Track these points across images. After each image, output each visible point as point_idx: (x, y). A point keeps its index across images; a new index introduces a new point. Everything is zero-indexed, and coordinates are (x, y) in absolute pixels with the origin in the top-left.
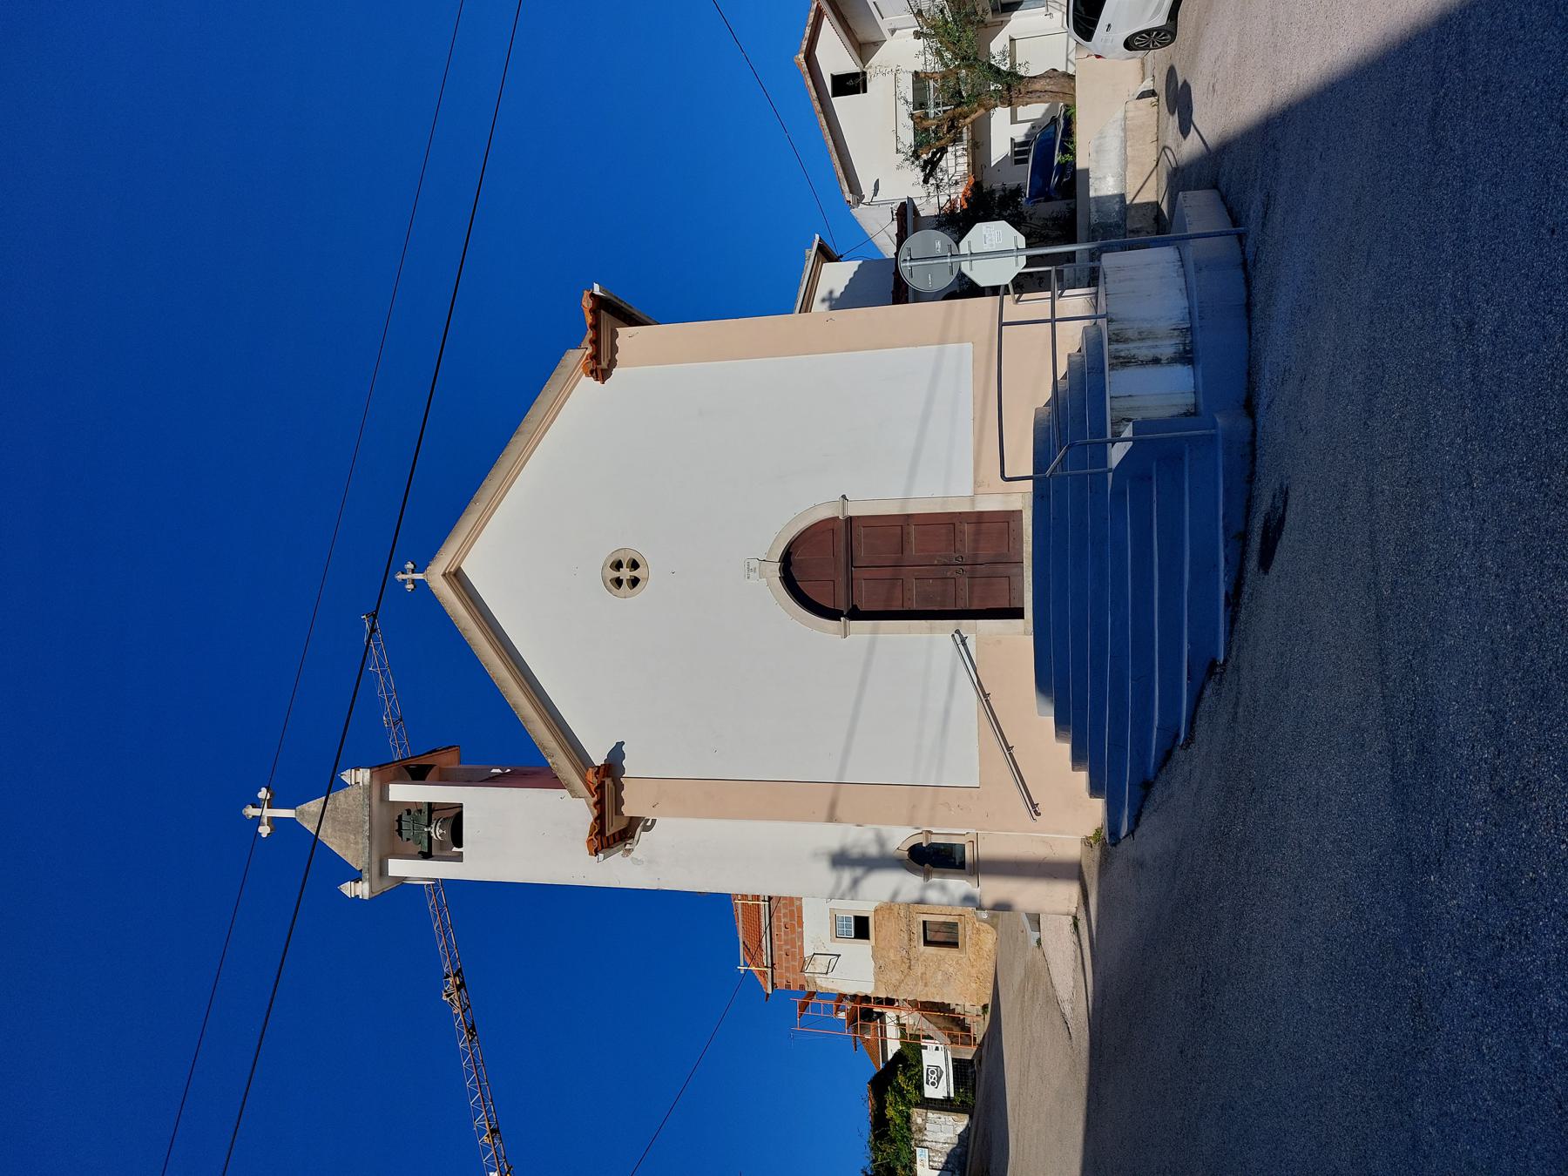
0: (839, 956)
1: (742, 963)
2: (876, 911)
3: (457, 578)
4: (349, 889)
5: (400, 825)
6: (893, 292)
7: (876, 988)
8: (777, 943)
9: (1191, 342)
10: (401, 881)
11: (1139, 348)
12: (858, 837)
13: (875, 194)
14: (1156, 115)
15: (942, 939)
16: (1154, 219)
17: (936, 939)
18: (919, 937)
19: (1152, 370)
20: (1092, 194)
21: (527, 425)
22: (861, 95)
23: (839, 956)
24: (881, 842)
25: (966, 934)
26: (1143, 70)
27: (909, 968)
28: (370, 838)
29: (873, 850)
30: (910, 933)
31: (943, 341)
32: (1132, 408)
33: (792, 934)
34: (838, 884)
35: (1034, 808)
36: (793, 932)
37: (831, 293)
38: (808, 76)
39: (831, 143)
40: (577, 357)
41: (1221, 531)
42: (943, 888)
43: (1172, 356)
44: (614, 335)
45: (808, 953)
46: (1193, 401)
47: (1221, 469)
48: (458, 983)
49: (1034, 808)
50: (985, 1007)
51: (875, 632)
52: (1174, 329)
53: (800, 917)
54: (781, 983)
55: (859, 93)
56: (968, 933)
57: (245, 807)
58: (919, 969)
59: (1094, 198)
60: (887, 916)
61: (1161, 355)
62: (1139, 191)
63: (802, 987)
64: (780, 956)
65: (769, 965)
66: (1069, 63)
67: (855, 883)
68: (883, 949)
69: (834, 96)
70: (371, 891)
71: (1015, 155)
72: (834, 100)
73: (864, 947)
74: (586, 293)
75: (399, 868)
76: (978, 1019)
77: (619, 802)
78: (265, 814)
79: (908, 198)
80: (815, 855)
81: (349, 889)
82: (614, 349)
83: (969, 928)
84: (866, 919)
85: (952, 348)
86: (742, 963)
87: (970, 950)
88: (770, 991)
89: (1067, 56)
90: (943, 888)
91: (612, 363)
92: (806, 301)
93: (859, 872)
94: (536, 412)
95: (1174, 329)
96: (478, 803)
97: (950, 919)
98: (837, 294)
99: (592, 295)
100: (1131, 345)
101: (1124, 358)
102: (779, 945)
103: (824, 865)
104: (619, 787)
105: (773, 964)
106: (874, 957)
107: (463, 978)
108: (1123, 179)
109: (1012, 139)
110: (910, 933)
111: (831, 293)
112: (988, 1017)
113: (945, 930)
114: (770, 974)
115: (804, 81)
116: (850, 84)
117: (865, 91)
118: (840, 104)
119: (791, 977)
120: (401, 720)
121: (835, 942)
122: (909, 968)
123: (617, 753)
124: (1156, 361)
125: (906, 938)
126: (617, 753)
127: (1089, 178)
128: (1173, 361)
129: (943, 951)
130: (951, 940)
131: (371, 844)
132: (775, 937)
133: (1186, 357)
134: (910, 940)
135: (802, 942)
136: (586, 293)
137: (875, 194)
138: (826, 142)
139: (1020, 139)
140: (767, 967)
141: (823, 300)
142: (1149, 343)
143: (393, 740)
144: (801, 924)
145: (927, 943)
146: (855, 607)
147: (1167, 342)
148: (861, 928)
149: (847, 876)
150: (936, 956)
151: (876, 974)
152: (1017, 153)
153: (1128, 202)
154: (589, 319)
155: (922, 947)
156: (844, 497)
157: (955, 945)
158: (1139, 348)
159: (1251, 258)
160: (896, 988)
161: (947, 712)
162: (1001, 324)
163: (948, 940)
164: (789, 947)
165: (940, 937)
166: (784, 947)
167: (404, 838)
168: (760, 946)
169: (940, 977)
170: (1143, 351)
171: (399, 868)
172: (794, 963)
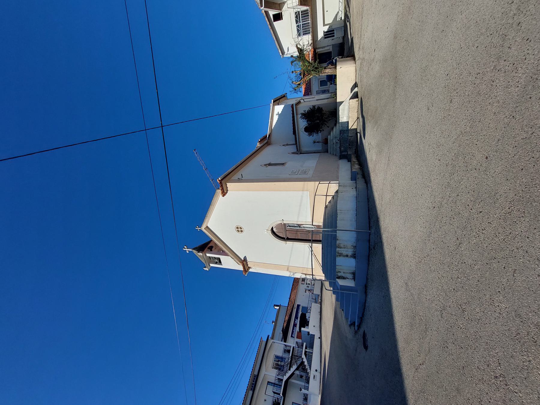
4: (205, 269)
6: (293, 129)
9: (356, 251)
10: (212, 267)
11: (344, 251)
13: (288, 51)
14: (358, 104)
16: (356, 134)
19: (346, 258)
20: (340, 121)
22: (281, 21)
26: (356, 72)
32: (341, 269)
37: (278, 113)
38: (266, 17)
39: (275, 38)
40: (219, 191)
41: (357, 316)
43: (351, 255)
44: (226, 185)
46: (355, 270)
47: (358, 301)
52: (352, 246)
55: (281, 20)
59: (341, 122)
61: (348, 254)
62: (352, 126)
66: (341, 11)
69: (274, 21)
70: (208, 269)
71: (325, 36)
72: (274, 23)
74: (218, 180)
75: (212, 265)
81: (205, 269)
82: (227, 188)
89: (339, 8)
91: (227, 191)
92: (271, 124)
95: (352, 246)
96: (222, 258)
98: (280, 113)
99: (219, 180)
100: (342, 249)
101: (340, 253)
104: (247, 263)
108: (349, 117)
109: (324, 31)
111: (278, 113)
115: (265, 19)
116: (278, 17)
117: (282, 19)
118: (276, 24)
123: (245, 258)
124: (347, 256)
126: (245, 258)
127: (339, 117)
128: (351, 256)
133: (354, 256)
136: (218, 180)
137: (288, 51)
138: (273, 38)
139: (326, 30)
141: (277, 115)
142: (346, 249)
146: (288, 237)
147: (350, 250)
152: (325, 35)
153: (349, 128)
156: (283, 220)
158: (344, 251)
159: (372, 247)
162: (315, 195)
170: (345, 253)
171: (212, 265)
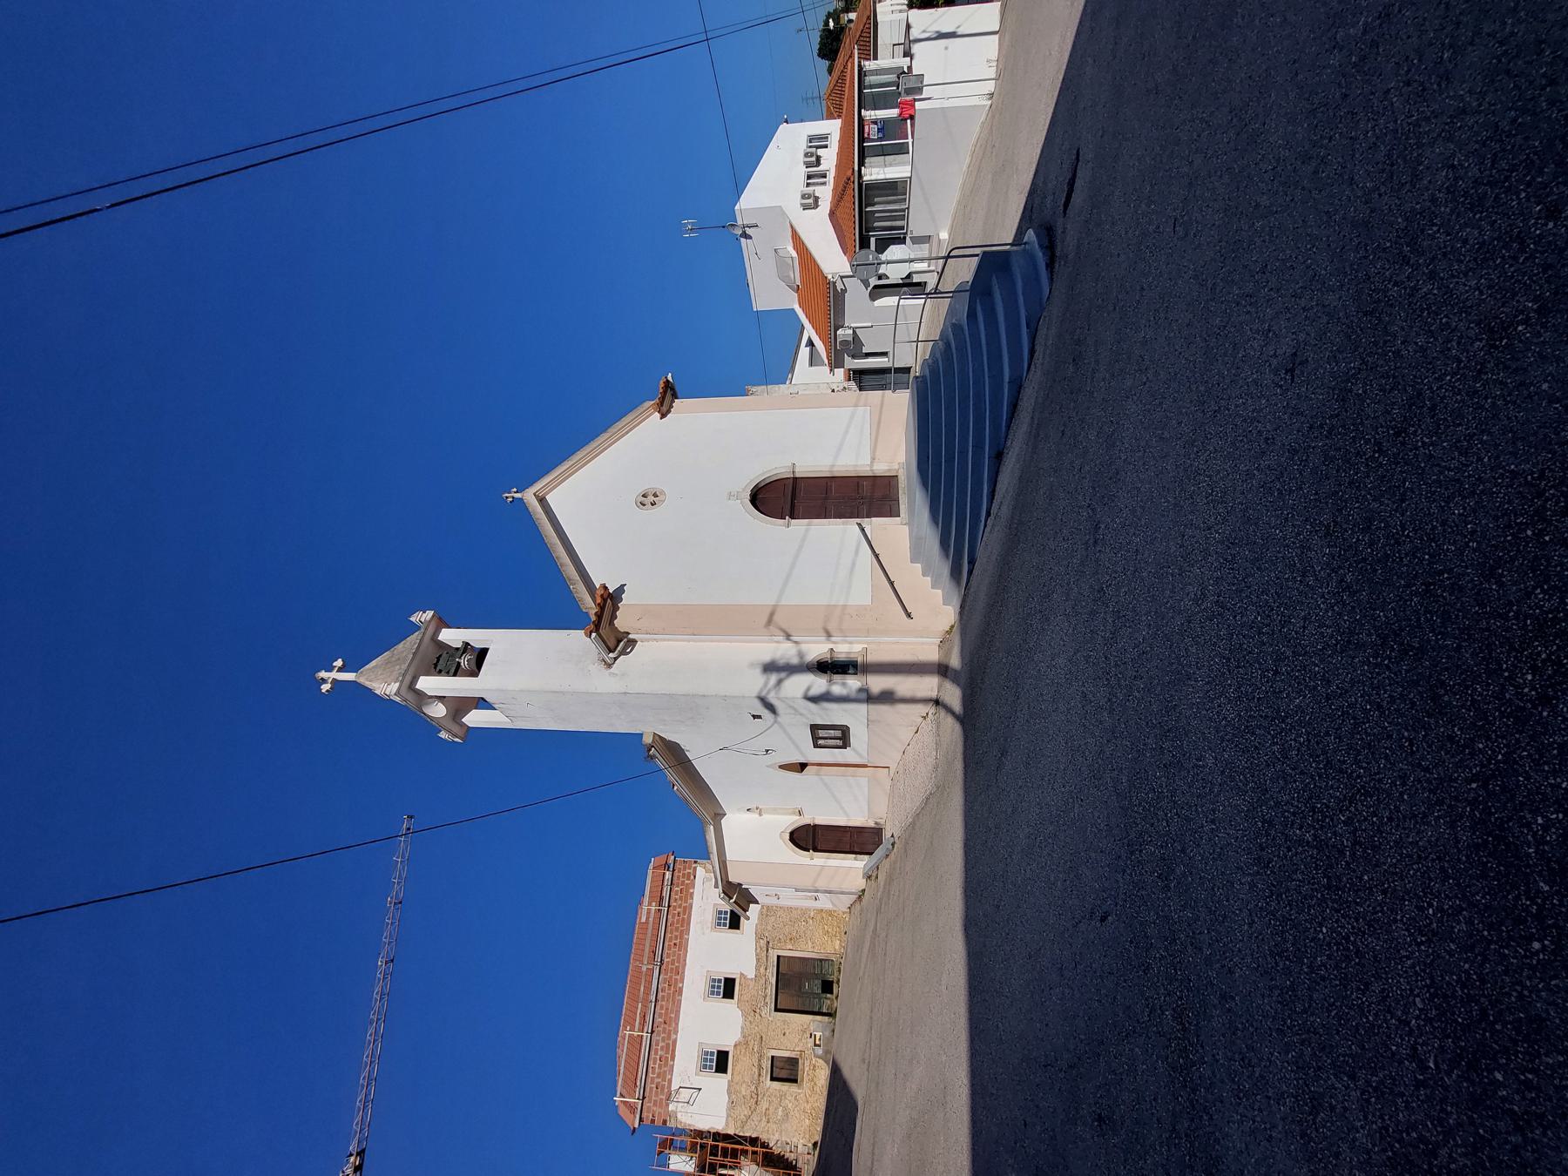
0: (700, 1089)
1: (618, 1094)
2: (735, 1046)
3: (542, 501)
5: (438, 661)
7: (727, 1125)
8: (651, 1075)
12: (784, 651)
15: (785, 1077)
17: (780, 1076)
18: (767, 1071)
21: (612, 430)
23: (700, 1089)
24: (801, 655)
25: (805, 1069)
27: (756, 1103)
28: (414, 654)
29: (795, 661)
30: (760, 1067)
31: (856, 405)
33: (665, 1066)
34: (766, 684)
35: (909, 615)
36: (666, 1065)
42: (844, 684)
45: (674, 1087)
48: (357, 1163)
49: (909, 615)
50: (815, 1144)
51: (809, 525)
53: (674, 1051)
54: (648, 1117)
56: (807, 1069)
57: (319, 671)
58: (764, 1105)
60: (743, 1051)
63: (665, 1122)
64: (651, 1088)
65: (650, 1031)
67: (780, 682)
68: (737, 1084)
73: (722, 1080)
76: (809, 1156)
77: (614, 617)
78: (332, 676)
79: (742, 974)
80: (752, 665)
83: (807, 1063)
84: (727, 1053)
85: (861, 409)
86: (618, 1094)
87: (806, 1084)
88: (636, 1126)
90: (844, 684)
91: (669, 411)
93: (783, 675)
94: (619, 424)
97: (793, 1055)
102: (653, 1079)
103: (758, 671)
105: (644, 1098)
106: (729, 1092)
107: (363, 1160)
110: (760, 1067)
112: (817, 1152)
113: (788, 1067)
114: (640, 1105)
119: (657, 1110)
120: (392, 961)
121: (699, 1075)
122: (756, 1103)
123: (621, 589)
125: (757, 1073)
126: (621, 589)
129: (785, 1087)
130: (792, 1077)
131: (413, 659)
132: (650, 1070)
134: (760, 1075)
135: (672, 1075)
140: (638, 1099)
143: (371, 1035)
144: (673, 1058)
145: (773, 1079)
148: (721, 1062)
149: (774, 678)
150: (780, 1091)
151: (729, 1109)
154: (661, 391)
155: (768, 1082)
157: (795, 1081)
160: (744, 1124)
161: (854, 564)
163: (789, 1077)
164: (660, 1080)
165: (783, 1074)
166: (657, 1080)
167: (438, 669)
168: (636, 1084)
169: (780, 1113)
172: (662, 1097)
